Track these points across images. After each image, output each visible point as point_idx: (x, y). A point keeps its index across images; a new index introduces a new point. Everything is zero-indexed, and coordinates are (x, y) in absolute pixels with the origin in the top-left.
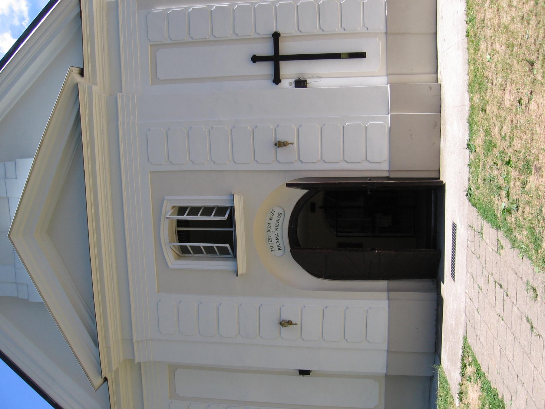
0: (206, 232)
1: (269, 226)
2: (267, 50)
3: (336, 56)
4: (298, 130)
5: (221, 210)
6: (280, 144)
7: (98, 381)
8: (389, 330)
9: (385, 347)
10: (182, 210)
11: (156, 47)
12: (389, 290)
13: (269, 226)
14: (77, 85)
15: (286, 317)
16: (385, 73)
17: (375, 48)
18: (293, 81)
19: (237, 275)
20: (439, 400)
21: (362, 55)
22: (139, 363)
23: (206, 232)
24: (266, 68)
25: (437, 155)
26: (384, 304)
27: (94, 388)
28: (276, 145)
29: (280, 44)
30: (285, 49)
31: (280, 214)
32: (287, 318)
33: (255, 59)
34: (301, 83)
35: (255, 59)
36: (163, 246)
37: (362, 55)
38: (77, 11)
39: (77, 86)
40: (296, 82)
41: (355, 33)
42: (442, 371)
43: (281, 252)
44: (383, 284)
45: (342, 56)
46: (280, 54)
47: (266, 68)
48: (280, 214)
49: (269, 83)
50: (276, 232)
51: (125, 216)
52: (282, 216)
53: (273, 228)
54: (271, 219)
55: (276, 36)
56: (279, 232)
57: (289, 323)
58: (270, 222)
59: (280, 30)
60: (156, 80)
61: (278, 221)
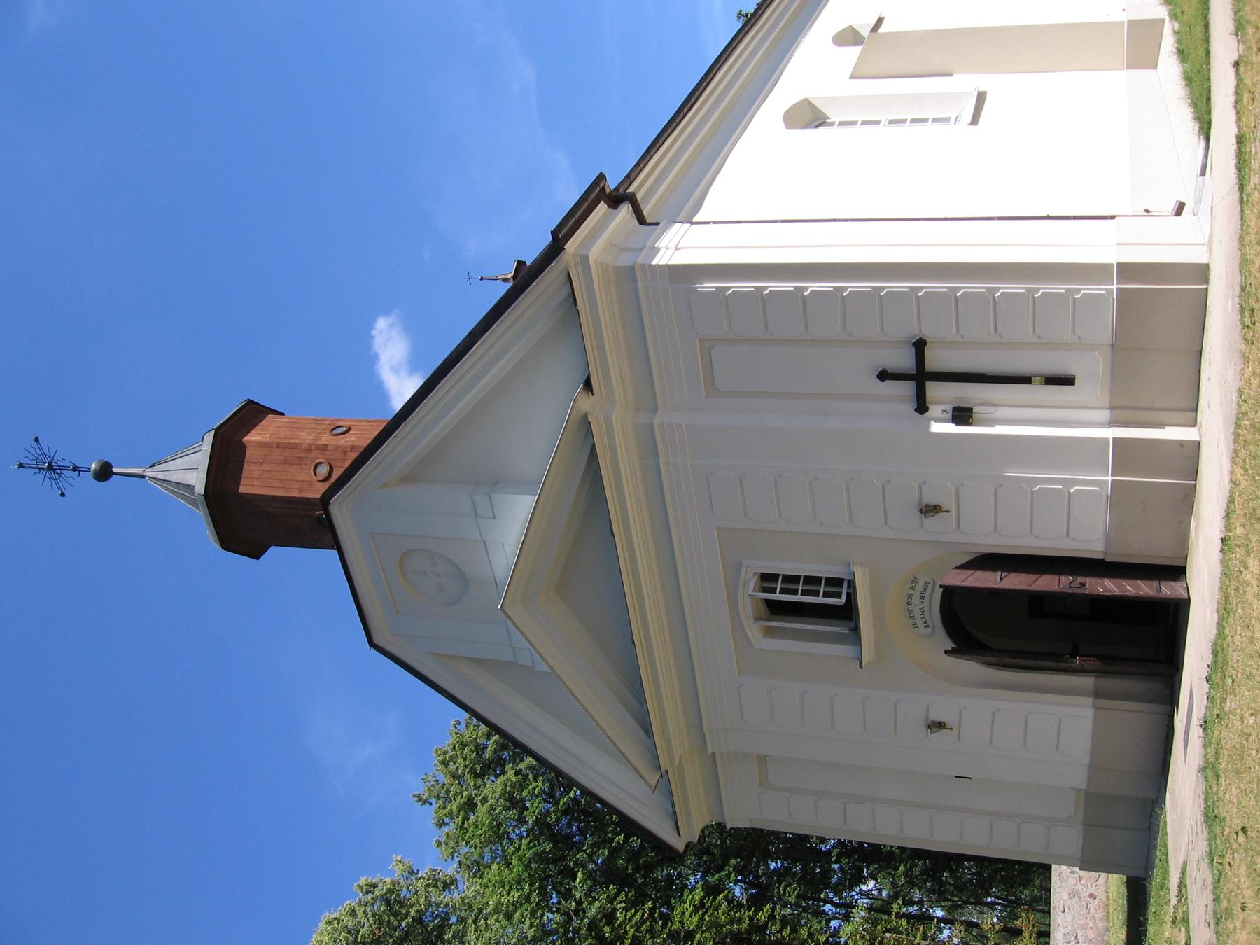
1: (910, 596)
2: (906, 361)
3: (1025, 380)
5: (835, 582)
6: (931, 510)
7: (653, 779)
9: (1087, 761)
10: (767, 580)
12: (1098, 694)
13: (910, 596)
14: (585, 416)
15: (936, 716)
16: (1107, 404)
17: (1092, 369)
18: (949, 408)
19: (861, 666)
20: (1157, 861)
22: (714, 754)
23: (812, 605)
25: (1183, 541)
26: (1090, 712)
27: (650, 786)
28: (921, 511)
31: (927, 583)
32: (938, 718)
35: (884, 376)
36: (745, 624)
37: (1068, 381)
38: (566, 291)
39: (585, 425)
40: (955, 409)
42: (1162, 887)
43: (929, 630)
48: (927, 583)
51: (691, 636)
52: (930, 587)
53: (916, 600)
54: (912, 588)
55: (920, 346)
56: (926, 605)
57: (941, 726)
58: (911, 592)
59: (927, 333)
61: (924, 592)
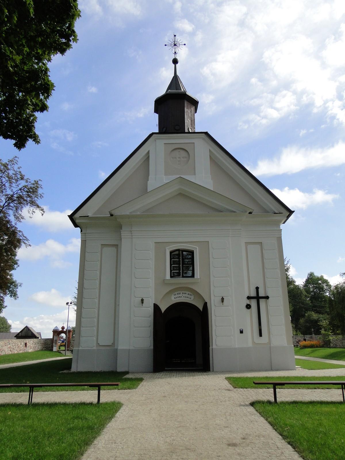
0: (182, 262)
2: (261, 294)
4: (216, 340)
8: (154, 322)
11: (272, 370)
21: (261, 335)
24: (253, 294)
29: (264, 299)
30: (262, 302)
33: (257, 288)
34: (248, 307)
35: (257, 288)
37: (261, 335)
41: (267, 304)
44: (152, 347)
45: (260, 327)
46: (260, 296)
47: (253, 294)
49: (247, 294)
50: (181, 293)
60: (247, 243)
